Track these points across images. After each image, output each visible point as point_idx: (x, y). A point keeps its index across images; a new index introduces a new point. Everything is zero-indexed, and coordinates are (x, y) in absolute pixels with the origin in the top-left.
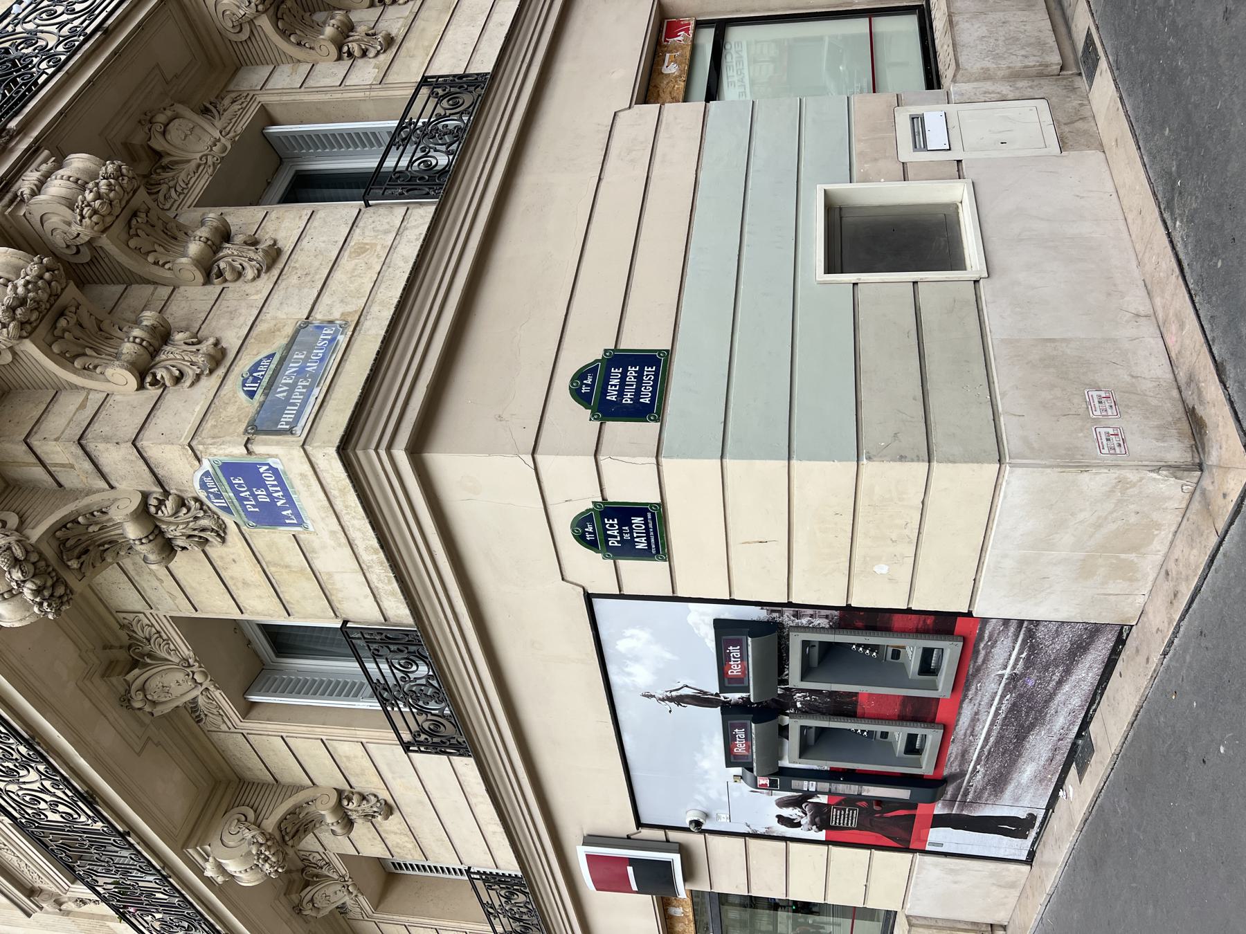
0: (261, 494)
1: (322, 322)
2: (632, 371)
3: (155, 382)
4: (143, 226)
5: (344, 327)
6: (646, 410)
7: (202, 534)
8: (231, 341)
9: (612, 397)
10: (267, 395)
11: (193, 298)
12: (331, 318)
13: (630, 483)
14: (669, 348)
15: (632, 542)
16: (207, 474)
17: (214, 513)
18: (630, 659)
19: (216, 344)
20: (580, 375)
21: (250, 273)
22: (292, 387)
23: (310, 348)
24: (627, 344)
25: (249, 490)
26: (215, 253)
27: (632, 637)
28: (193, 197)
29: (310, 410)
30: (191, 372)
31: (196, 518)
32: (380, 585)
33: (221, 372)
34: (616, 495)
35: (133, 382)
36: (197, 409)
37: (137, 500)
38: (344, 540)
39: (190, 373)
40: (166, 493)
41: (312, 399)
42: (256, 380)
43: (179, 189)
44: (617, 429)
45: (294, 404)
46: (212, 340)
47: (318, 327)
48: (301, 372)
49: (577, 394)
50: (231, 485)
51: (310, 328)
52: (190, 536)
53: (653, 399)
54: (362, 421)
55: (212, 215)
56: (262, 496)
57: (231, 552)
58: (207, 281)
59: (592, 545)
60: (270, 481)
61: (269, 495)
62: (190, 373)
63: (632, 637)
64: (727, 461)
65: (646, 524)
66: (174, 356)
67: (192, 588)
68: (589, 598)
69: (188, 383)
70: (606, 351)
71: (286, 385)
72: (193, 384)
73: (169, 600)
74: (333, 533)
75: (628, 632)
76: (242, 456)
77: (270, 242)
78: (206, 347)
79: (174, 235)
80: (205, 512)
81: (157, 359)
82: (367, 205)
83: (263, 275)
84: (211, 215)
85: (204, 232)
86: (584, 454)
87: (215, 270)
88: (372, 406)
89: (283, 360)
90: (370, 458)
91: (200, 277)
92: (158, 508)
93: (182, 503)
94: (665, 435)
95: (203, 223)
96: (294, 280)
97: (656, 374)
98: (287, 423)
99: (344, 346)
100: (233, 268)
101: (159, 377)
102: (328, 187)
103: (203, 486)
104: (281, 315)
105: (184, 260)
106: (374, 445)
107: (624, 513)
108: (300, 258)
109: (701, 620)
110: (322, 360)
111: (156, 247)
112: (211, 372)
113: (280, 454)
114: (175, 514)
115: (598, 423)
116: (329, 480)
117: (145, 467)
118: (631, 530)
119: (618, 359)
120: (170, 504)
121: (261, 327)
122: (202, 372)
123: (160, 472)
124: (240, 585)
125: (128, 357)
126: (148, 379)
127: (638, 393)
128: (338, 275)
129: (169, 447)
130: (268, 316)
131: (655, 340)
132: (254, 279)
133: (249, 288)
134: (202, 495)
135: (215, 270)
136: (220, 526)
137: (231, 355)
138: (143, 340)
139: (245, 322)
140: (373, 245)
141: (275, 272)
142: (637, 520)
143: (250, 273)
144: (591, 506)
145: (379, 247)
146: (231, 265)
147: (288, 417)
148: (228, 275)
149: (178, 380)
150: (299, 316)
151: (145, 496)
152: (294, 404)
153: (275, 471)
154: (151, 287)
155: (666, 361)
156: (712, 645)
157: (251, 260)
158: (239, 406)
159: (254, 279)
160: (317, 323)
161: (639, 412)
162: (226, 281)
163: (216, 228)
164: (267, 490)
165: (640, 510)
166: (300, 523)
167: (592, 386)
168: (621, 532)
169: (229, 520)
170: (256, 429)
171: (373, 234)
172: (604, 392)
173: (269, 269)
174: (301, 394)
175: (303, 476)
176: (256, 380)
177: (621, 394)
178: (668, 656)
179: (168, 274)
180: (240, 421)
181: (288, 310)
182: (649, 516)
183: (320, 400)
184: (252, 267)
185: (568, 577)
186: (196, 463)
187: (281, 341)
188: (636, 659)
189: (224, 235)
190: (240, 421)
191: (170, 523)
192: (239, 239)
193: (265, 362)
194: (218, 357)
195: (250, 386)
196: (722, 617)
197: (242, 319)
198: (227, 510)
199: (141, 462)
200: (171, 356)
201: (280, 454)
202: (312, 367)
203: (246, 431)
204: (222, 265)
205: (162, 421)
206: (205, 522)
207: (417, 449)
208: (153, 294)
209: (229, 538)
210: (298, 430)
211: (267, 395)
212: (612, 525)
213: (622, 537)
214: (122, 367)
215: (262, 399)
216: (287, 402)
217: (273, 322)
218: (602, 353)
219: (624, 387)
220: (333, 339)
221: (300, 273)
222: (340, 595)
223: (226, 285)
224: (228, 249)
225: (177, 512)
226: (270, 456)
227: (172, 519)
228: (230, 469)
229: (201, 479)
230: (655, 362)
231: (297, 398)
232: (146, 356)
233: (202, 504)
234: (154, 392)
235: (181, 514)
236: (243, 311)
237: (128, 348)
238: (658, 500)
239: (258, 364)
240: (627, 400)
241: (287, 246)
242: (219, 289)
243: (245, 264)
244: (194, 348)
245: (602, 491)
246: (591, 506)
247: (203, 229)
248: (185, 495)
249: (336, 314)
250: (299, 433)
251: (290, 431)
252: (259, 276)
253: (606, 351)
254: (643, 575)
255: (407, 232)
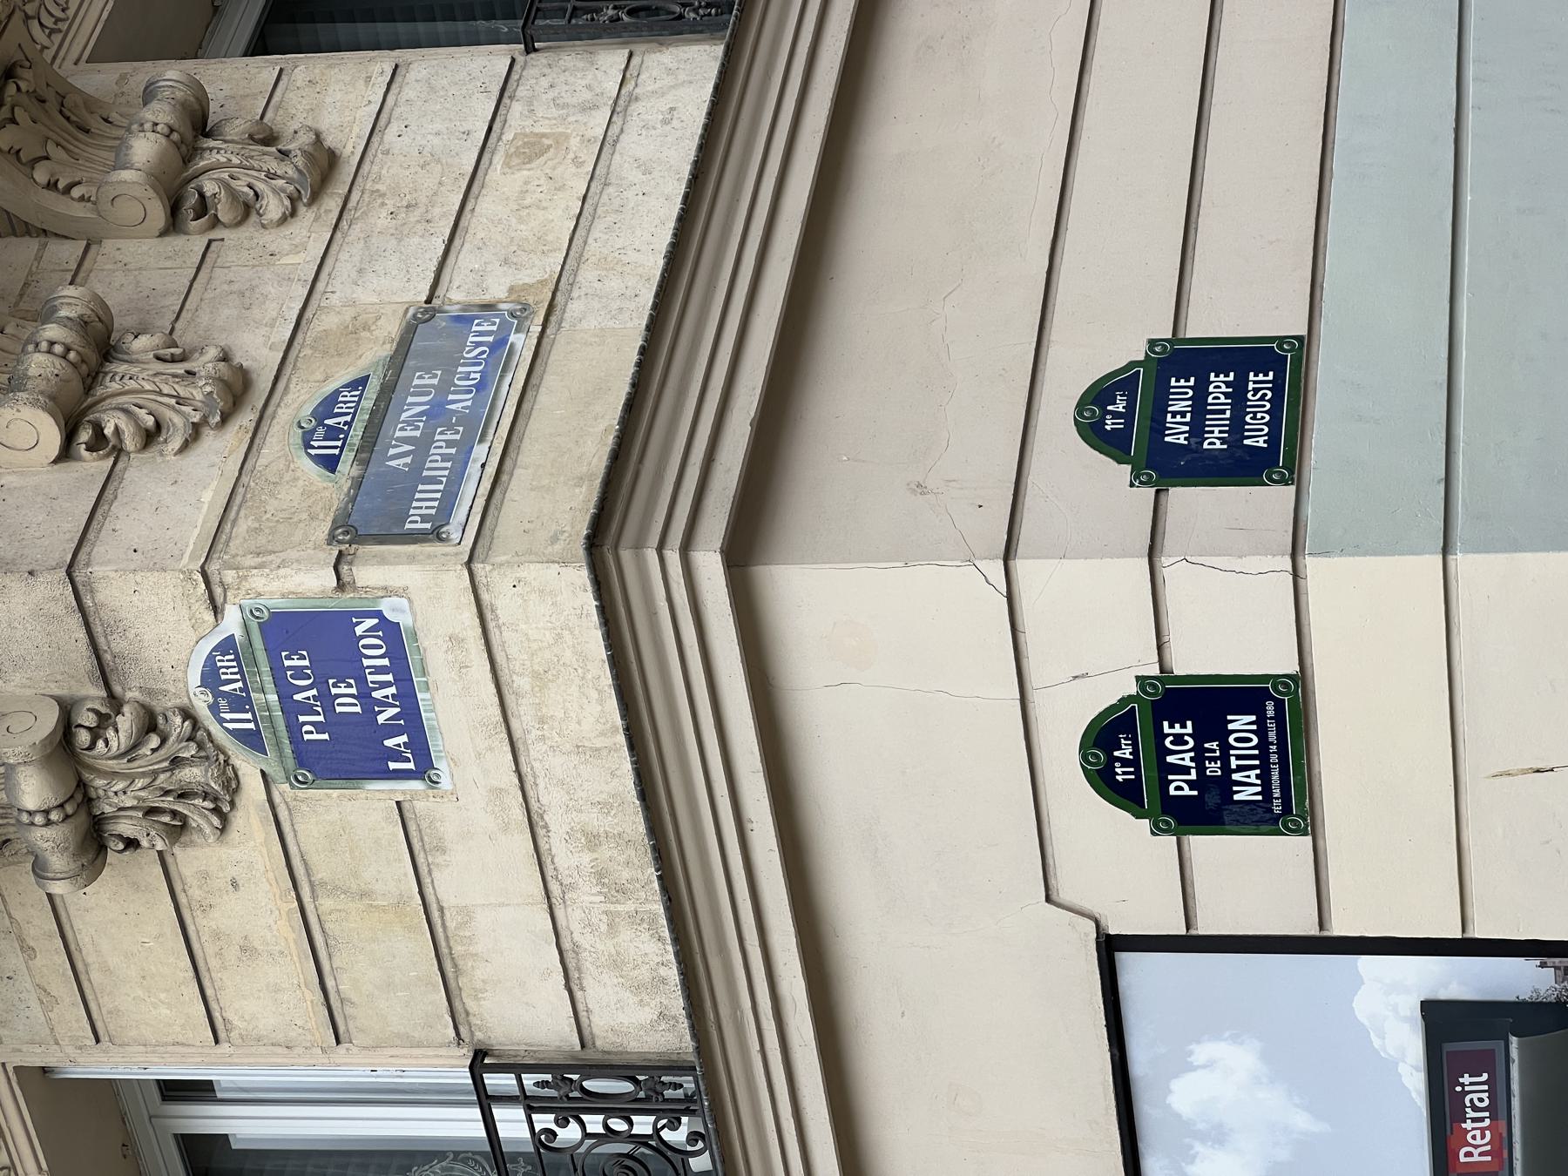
0: (346, 701)
1: (467, 307)
2: (1219, 385)
3: (98, 442)
4: (24, 99)
5: (521, 314)
6: (1265, 461)
7: (179, 808)
8: (258, 350)
9: (1177, 435)
10: (366, 463)
11: (140, 267)
12: (487, 298)
13: (1227, 636)
14: (1303, 332)
15: (1225, 784)
16: (227, 646)
17: (220, 749)
18: (1203, 1137)
19: (225, 358)
20: (1099, 395)
21: (273, 207)
22: (422, 447)
23: (450, 363)
24: (1199, 327)
25: (320, 683)
26: (187, 160)
27: (1209, 1065)
28: (81, 40)
29: (472, 490)
30: (178, 420)
31: (176, 762)
32: (585, 940)
33: (246, 419)
34: (1191, 661)
35: (52, 437)
36: (207, 497)
37: (49, 719)
38: (519, 814)
39: (177, 423)
40: (115, 702)
41: (473, 469)
42: (332, 433)
43: (48, 21)
44: (1192, 503)
45: (433, 480)
46: (212, 353)
47: (458, 319)
48: (437, 414)
49: (1093, 433)
50: (278, 672)
51: (440, 322)
52: (151, 811)
53: (1273, 439)
54: (625, 490)
55: (172, 73)
56: (346, 701)
57: (234, 869)
58: (174, 224)
59: (1125, 795)
60: (374, 656)
61: (364, 696)
62: (177, 423)
63: (1209, 1065)
64: (1459, 560)
65: (1261, 732)
66: (135, 385)
67: (106, 970)
68: (1110, 947)
69: (176, 443)
70: (1152, 343)
71: (406, 440)
72: (185, 446)
73: (37, 1010)
74: (498, 792)
75: (1202, 1052)
76: (324, 596)
77: (306, 139)
78: (205, 363)
79: (81, 122)
80: (200, 747)
81: (99, 392)
82: (530, 49)
83: (302, 210)
84: (171, 74)
85: (161, 113)
86: (1124, 554)
87: (192, 200)
88: (641, 460)
89: (388, 391)
90: (649, 570)
91: (158, 214)
92: (96, 733)
93: (150, 724)
94: (1309, 510)
95: (149, 94)
96: (381, 220)
97: (1277, 388)
98: (424, 519)
99: (528, 355)
100: (233, 194)
101: (108, 431)
102: (352, 19)
103: (211, 678)
104: (365, 296)
105: (126, 175)
106: (654, 540)
107: (1204, 703)
108: (387, 172)
109: (1390, 996)
110: (481, 386)
111: (51, 147)
112: (225, 419)
113: (413, 589)
114: (131, 752)
115: (1150, 492)
116: (513, 651)
117: (82, 634)
118: (1226, 748)
119: (1181, 358)
120: (126, 722)
121: (324, 323)
122: (205, 420)
123: (115, 645)
124: (232, 953)
125: (43, 385)
126: (85, 435)
127: (1237, 426)
128: (486, 206)
129: (154, 577)
130: (335, 300)
131: (1279, 319)
132: (283, 220)
133: (275, 240)
134: (201, 703)
135: (192, 200)
136: (226, 786)
137: (263, 383)
138: (68, 349)
139: (281, 314)
140: (560, 140)
141: (331, 204)
142: (1241, 723)
143: (273, 207)
144: (1133, 689)
145: (574, 142)
146: (227, 186)
147: (425, 503)
148: (224, 212)
149: (151, 436)
150: (408, 297)
151: (67, 709)
152: (433, 480)
153: (390, 632)
154: (33, 244)
155: (1297, 361)
156: (1414, 1081)
157: (271, 176)
158: (305, 490)
159: (283, 220)
160: (454, 310)
161: (1243, 466)
162: (216, 222)
163: (184, 105)
164: (361, 681)
165: (1246, 694)
166: (424, 768)
167: (1128, 415)
168: (1200, 757)
169: (248, 767)
170: (355, 531)
171: (554, 112)
172: (1158, 427)
173: (315, 197)
174: (445, 458)
175: (455, 640)
176: (332, 433)
177: (1197, 430)
178: (1302, 1121)
179: (80, 211)
180: (313, 518)
181: (380, 282)
182: (1270, 712)
183: (491, 470)
184: (275, 191)
185: (1064, 894)
186: (209, 617)
187: (373, 353)
188: (1218, 1136)
189: (197, 125)
190: (313, 518)
191: (115, 775)
192: (236, 129)
193: (347, 396)
194: (236, 389)
195: (322, 446)
196: (1443, 995)
197: (271, 309)
198: (251, 740)
199: (75, 621)
200: (132, 385)
201: (413, 589)
202: (460, 403)
203: (332, 539)
204: (210, 188)
205: (129, 522)
206: (192, 775)
207: (741, 555)
208: (38, 258)
209: (238, 820)
210: (453, 529)
211: (366, 463)
212: (1179, 740)
213: (1201, 769)
214: (34, 404)
215: (356, 471)
216: (415, 475)
217: (348, 314)
218: (1144, 347)
219: (1203, 416)
220: (500, 343)
221: (390, 204)
222: (479, 974)
223: (216, 234)
224: (216, 154)
225: (135, 747)
226: (388, 592)
227: (120, 765)
228: (284, 629)
229: (210, 659)
230: (1279, 364)
231: (437, 464)
232: (76, 385)
233: (196, 724)
234: (93, 467)
235: (145, 750)
236: (272, 290)
237: (39, 365)
238: (1293, 668)
239: (332, 399)
240: (1214, 440)
241: (349, 145)
242: (199, 243)
243: (260, 186)
244: (179, 369)
245: (1160, 647)
246: (1133, 689)
247: (155, 105)
248: (158, 707)
249: (496, 290)
250: (455, 536)
251: (436, 535)
252: (293, 213)
253: (1152, 343)
254: (1246, 877)
255: (635, 108)
